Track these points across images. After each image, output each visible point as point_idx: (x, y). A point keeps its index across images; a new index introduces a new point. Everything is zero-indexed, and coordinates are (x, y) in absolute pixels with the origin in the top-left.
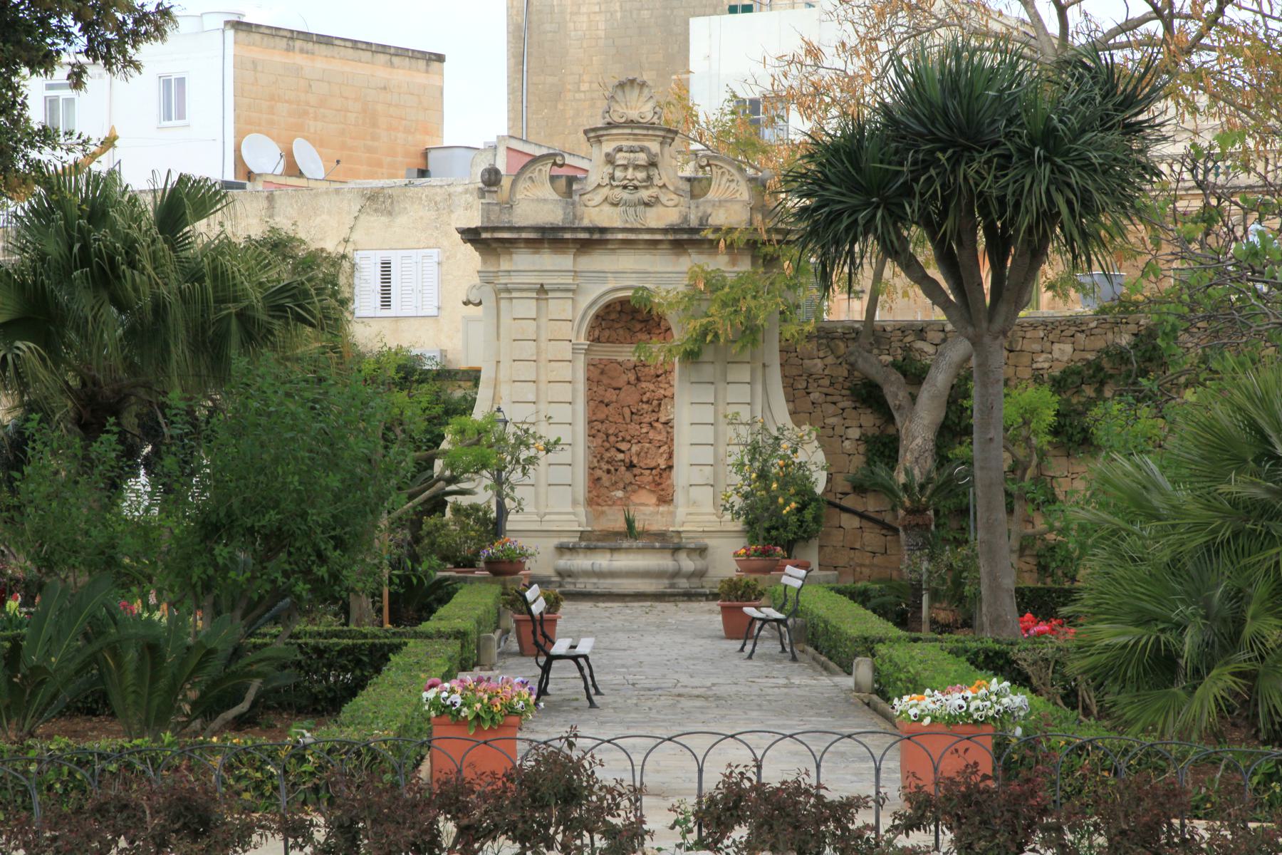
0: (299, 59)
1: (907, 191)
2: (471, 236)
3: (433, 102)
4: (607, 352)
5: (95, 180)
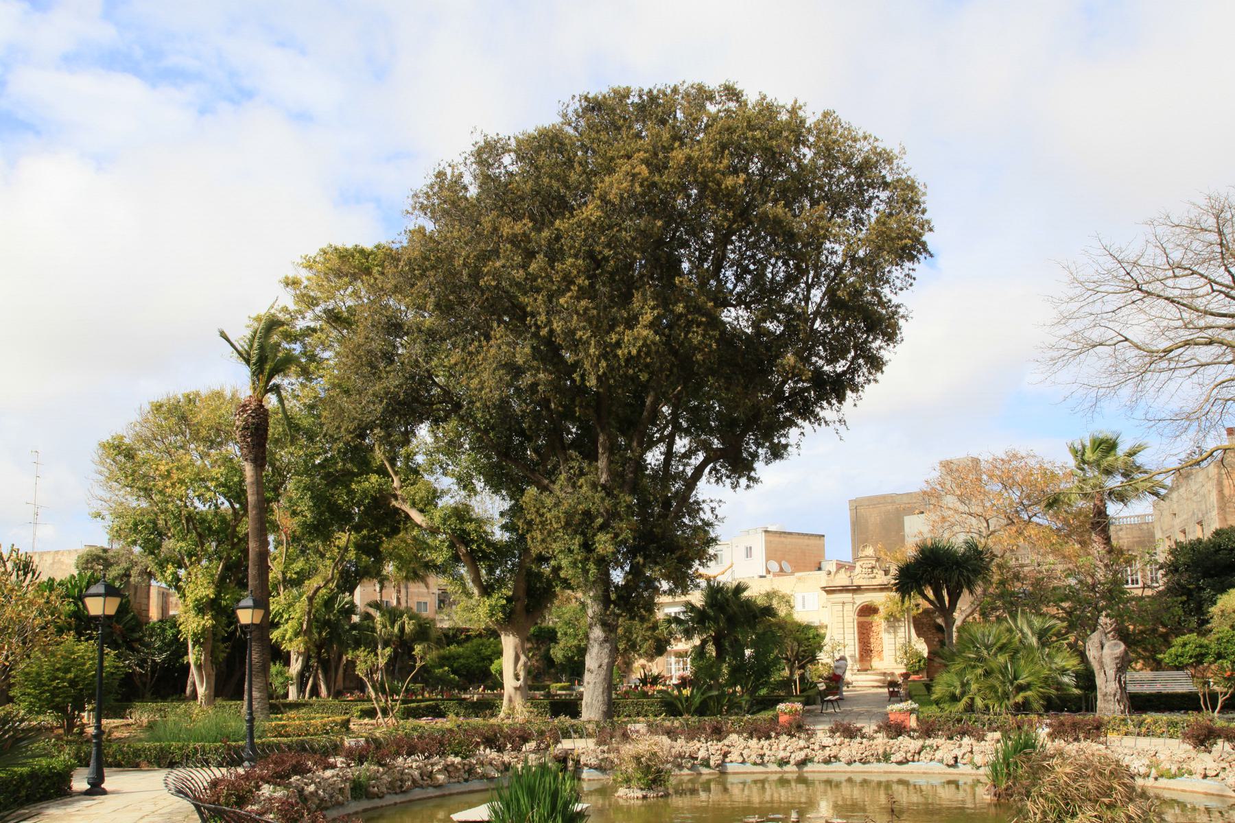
0: (783, 539)
1: (921, 578)
2: (824, 588)
4: (863, 619)
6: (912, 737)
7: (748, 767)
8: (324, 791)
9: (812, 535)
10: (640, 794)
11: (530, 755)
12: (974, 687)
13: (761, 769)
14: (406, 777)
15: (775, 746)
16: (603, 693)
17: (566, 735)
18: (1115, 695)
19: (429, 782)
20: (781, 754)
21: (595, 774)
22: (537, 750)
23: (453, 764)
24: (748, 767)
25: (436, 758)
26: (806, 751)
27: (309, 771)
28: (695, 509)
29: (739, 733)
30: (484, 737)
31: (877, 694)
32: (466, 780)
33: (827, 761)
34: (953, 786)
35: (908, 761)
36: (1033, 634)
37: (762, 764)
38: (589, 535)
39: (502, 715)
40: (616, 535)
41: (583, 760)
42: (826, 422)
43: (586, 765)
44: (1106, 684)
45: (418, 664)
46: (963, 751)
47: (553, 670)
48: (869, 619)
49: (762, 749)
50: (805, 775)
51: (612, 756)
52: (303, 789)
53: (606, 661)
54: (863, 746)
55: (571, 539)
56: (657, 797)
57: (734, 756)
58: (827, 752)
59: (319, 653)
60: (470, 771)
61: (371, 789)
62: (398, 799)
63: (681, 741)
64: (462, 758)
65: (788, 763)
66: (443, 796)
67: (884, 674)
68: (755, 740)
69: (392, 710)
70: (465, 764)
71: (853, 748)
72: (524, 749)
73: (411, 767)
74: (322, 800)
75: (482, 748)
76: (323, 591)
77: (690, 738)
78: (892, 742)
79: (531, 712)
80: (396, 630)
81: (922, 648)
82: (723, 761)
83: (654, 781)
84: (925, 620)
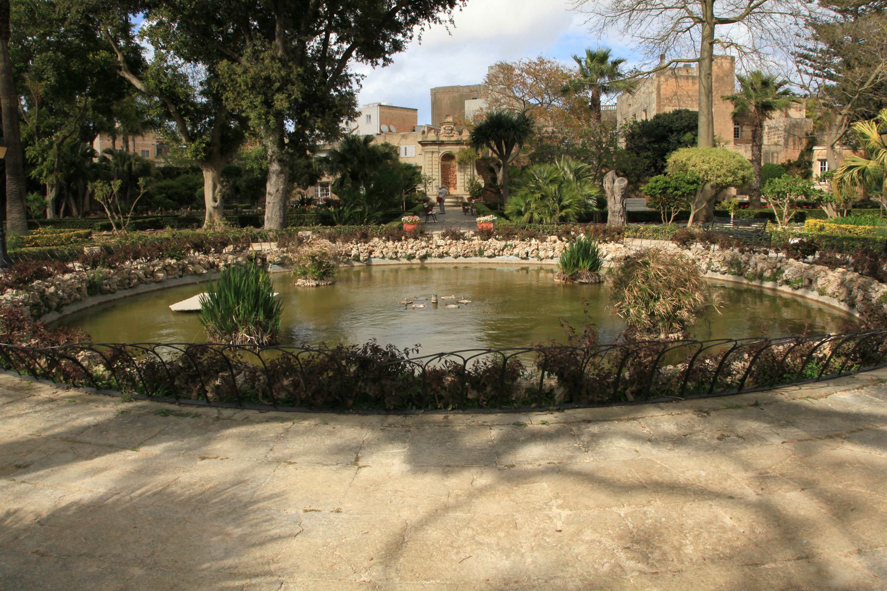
0: (391, 111)
1: (490, 135)
2: (420, 143)
3: (415, 118)
4: (444, 163)
5: (353, 136)
6: (497, 239)
7: (387, 261)
8: (63, 291)
9: (410, 109)
10: (314, 283)
11: (229, 256)
12: (533, 206)
13: (395, 262)
14: (132, 276)
15: (405, 246)
16: (280, 209)
17: (255, 240)
18: (619, 212)
19: (152, 279)
20: (410, 252)
21: (277, 269)
22: (234, 252)
23: (170, 264)
24: (387, 261)
25: (156, 261)
26: (426, 249)
27: (50, 275)
28: (345, 80)
29: (380, 237)
30: (194, 244)
31: (453, 211)
32: (181, 276)
33: (441, 256)
34: (525, 271)
35: (495, 256)
36: (571, 172)
37: (397, 258)
38: (269, 95)
39: (205, 226)
40: (290, 96)
41: (268, 258)
42: (440, 21)
43: (270, 262)
44: (614, 205)
45: (142, 191)
46: (532, 249)
47: (238, 196)
48: (448, 163)
49: (396, 248)
50: (426, 266)
51: (290, 255)
52: (44, 290)
53: (282, 187)
54: (465, 245)
55: (255, 98)
56: (327, 284)
57: (377, 253)
58: (441, 249)
59: (68, 186)
60: (184, 269)
61: (104, 287)
62: (128, 293)
63: (339, 244)
64: (177, 260)
65: (414, 257)
66: (163, 289)
67: (457, 198)
68: (391, 242)
69: (125, 225)
70: (179, 264)
71: (458, 247)
72: (224, 251)
73: (137, 268)
74: (62, 298)
75: (192, 251)
76: (68, 140)
77: (346, 241)
78: (485, 242)
79: (226, 224)
80: (125, 167)
81: (481, 182)
82: (369, 257)
83: (324, 274)
84: (483, 165)
